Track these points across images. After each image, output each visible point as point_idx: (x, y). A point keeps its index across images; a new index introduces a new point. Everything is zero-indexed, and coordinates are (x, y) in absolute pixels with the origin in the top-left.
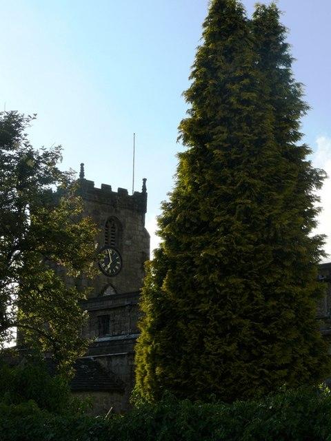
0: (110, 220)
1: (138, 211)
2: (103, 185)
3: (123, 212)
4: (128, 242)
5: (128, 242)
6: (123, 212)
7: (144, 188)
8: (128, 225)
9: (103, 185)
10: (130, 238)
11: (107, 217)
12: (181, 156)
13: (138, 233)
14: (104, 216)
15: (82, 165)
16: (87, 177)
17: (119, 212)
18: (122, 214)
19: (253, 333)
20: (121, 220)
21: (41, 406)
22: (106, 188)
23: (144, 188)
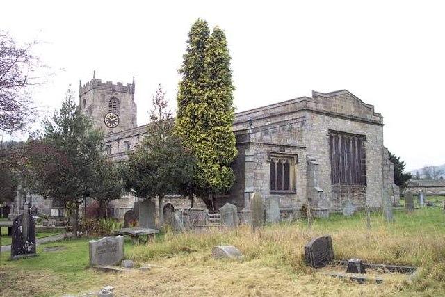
4: (123, 109)
5: (123, 109)
8: (122, 101)
14: (108, 97)
18: (119, 96)
22: (110, 83)
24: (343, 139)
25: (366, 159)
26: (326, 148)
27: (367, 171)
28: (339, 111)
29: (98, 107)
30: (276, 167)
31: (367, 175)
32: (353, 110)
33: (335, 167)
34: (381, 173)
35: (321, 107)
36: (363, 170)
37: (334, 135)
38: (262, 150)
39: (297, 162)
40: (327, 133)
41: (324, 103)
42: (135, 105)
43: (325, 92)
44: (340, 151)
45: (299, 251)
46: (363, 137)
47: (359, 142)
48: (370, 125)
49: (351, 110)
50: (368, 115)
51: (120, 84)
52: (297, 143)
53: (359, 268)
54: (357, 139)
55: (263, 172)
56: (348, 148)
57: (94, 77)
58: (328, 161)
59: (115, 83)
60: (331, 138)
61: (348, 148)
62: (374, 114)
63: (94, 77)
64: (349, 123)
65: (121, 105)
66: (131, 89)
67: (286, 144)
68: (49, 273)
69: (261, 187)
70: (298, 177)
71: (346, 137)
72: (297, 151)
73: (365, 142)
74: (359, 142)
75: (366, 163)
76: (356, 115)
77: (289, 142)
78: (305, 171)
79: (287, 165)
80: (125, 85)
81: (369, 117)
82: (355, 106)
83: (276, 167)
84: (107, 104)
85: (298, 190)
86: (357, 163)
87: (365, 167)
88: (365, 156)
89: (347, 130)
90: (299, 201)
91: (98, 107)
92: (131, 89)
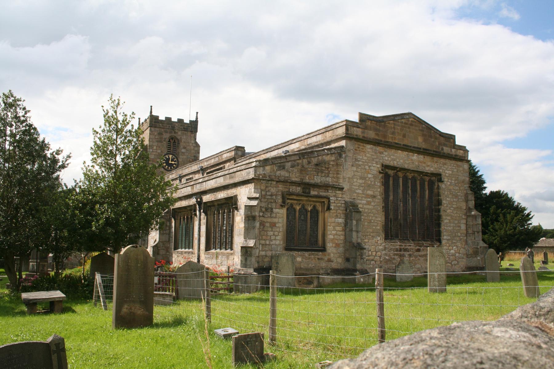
0: (172, 138)
1: (191, 132)
2: (166, 118)
3: (180, 133)
4: (183, 150)
5: (183, 150)
6: (180, 133)
7: (197, 118)
8: (183, 140)
9: (166, 118)
10: (185, 148)
11: (168, 136)
12: (514, 202)
13: (191, 144)
14: (167, 136)
15: (151, 107)
16: (154, 114)
17: (177, 133)
18: (179, 134)
19: (67, 200)
20: (179, 137)
21: (104, 305)
22: (168, 119)
23: (197, 118)
24: (405, 179)
25: (442, 208)
26: (378, 189)
27: (443, 224)
28: (398, 139)
29: (155, 148)
30: (297, 214)
31: (443, 228)
32: (420, 139)
33: (391, 216)
34: (463, 227)
35: (371, 134)
36: (437, 221)
37: (391, 172)
38: (273, 190)
39: (329, 209)
40: (380, 169)
41: (375, 130)
42: (198, 146)
43: (442, 131)
44: (401, 195)
45: (68, 344)
46: (438, 177)
47: (431, 184)
48: (447, 161)
49: (420, 142)
50: (444, 148)
51: (180, 121)
52: (329, 180)
53: (420, 342)
54: (427, 179)
55: (275, 220)
56: (414, 191)
57: (151, 112)
58: (380, 208)
59: (174, 119)
60: (386, 177)
61: (414, 191)
62: (454, 146)
63: (151, 112)
64: (415, 157)
65: (182, 144)
66: (193, 126)
67: (312, 182)
68: (550, 301)
69: (271, 240)
70: (330, 228)
71: (427, 179)
72: (330, 193)
73: (440, 184)
74: (431, 184)
75: (442, 213)
76: (424, 146)
77: (318, 179)
78: (341, 220)
79: (315, 213)
80: (187, 121)
81: (446, 150)
82: (423, 135)
83: (297, 214)
84: (165, 144)
85: (329, 245)
86: (427, 212)
87: (439, 217)
88: (439, 203)
89: (411, 167)
90: (330, 260)
91: (155, 148)
92: (193, 126)
